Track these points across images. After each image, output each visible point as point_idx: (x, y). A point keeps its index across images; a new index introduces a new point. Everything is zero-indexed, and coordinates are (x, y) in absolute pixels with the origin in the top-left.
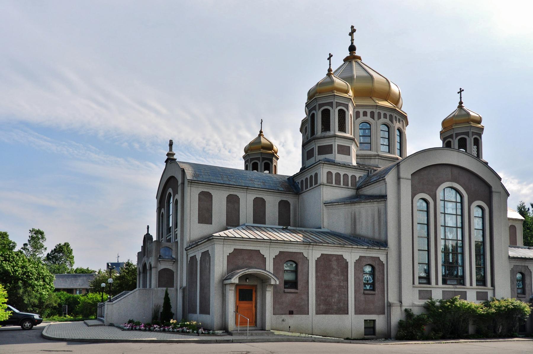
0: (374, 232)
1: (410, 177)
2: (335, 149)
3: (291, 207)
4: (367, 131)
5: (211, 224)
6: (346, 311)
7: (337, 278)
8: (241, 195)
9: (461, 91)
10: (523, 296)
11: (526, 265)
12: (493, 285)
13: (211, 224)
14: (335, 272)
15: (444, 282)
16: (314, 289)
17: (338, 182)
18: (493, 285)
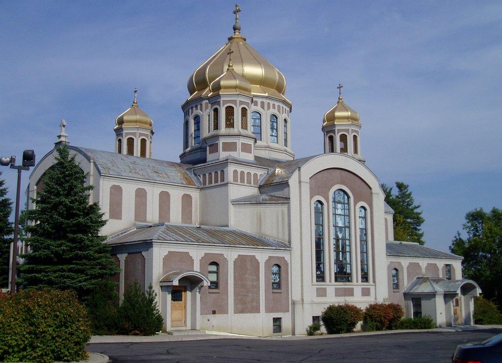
0: (278, 232)
1: (308, 181)
2: (239, 147)
3: (193, 201)
4: (257, 120)
5: (121, 219)
6: (257, 310)
7: (251, 277)
8: (147, 187)
9: (340, 87)
10: (397, 290)
11: (400, 261)
12: (374, 281)
13: (121, 219)
14: (249, 272)
15: (336, 280)
16: (233, 289)
17: (242, 180)
18: (374, 281)
